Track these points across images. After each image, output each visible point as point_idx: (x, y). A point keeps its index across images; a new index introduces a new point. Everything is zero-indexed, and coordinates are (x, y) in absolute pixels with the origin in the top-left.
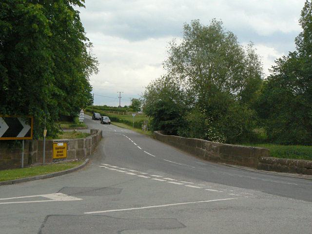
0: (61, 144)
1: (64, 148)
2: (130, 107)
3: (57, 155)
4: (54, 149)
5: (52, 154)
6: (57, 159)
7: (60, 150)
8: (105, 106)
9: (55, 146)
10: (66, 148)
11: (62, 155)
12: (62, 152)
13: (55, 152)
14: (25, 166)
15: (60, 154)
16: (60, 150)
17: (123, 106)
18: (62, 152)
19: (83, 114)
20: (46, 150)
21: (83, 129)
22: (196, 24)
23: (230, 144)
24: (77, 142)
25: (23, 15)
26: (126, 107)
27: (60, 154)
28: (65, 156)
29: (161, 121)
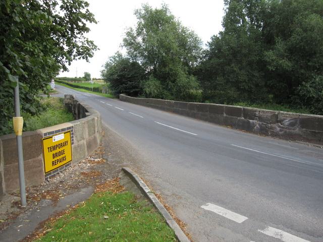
0: (59, 138)
1: (65, 144)
2: (83, 78)
3: (54, 163)
4: (46, 150)
5: (40, 164)
6: (55, 170)
7: (58, 150)
8: (65, 78)
9: (47, 144)
10: (69, 143)
11: (64, 159)
12: (62, 153)
13: (49, 157)
14: (20, 96)
15: (58, 158)
16: (58, 150)
17: (78, 77)
18: (62, 153)
19: (54, 82)
20: (25, 158)
21: (54, 94)
22: (146, 9)
23: (224, 104)
24: (86, 125)
25: (12, 17)
26: (80, 78)
27: (58, 158)
28: (68, 159)
29: (193, 78)
